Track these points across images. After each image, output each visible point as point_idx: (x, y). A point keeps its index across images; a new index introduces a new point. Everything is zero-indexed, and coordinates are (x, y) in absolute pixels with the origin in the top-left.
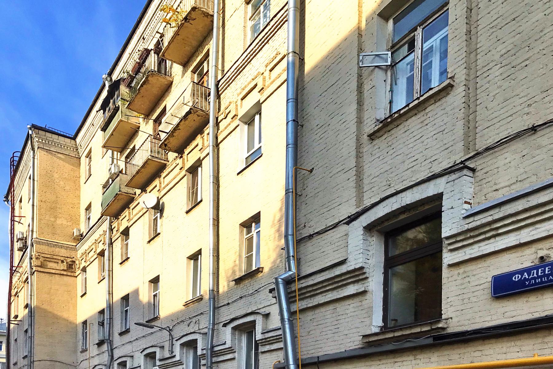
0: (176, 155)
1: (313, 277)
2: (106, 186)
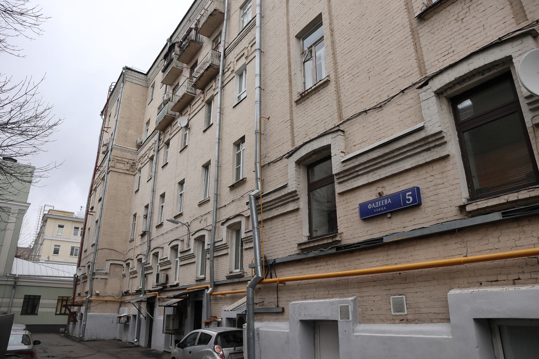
0: (200, 91)
1: (270, 196)
2: (160, 108)
